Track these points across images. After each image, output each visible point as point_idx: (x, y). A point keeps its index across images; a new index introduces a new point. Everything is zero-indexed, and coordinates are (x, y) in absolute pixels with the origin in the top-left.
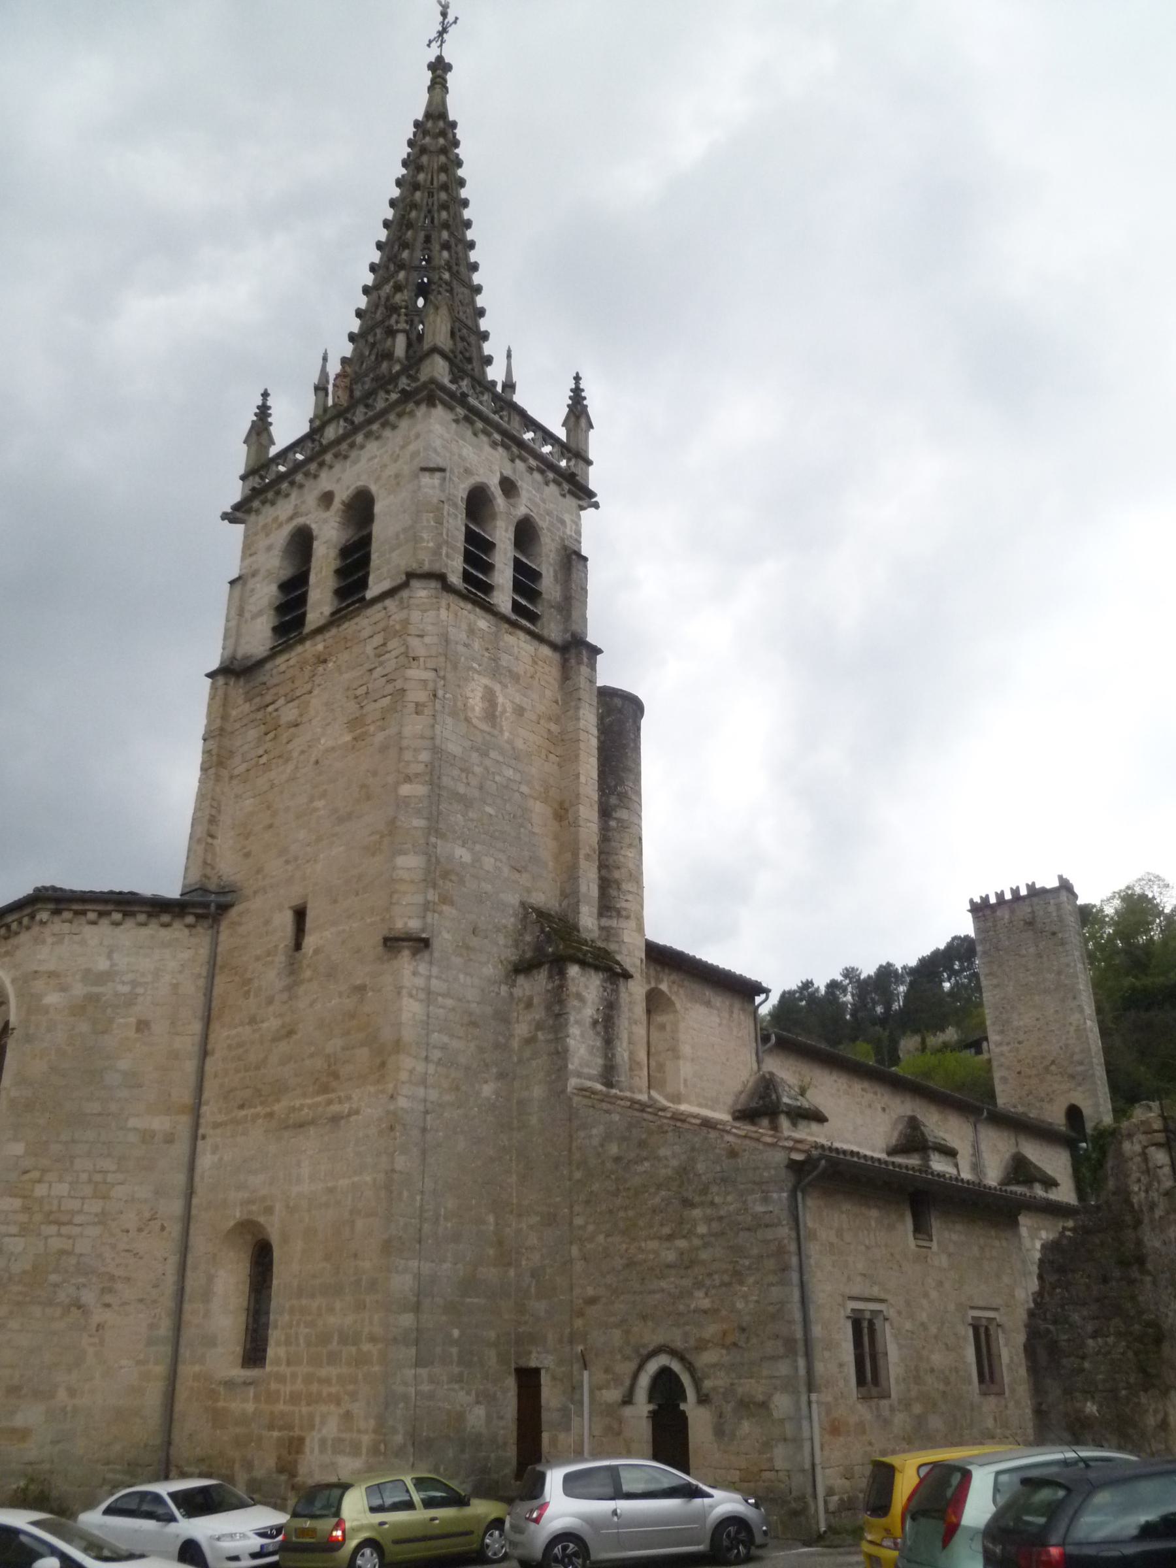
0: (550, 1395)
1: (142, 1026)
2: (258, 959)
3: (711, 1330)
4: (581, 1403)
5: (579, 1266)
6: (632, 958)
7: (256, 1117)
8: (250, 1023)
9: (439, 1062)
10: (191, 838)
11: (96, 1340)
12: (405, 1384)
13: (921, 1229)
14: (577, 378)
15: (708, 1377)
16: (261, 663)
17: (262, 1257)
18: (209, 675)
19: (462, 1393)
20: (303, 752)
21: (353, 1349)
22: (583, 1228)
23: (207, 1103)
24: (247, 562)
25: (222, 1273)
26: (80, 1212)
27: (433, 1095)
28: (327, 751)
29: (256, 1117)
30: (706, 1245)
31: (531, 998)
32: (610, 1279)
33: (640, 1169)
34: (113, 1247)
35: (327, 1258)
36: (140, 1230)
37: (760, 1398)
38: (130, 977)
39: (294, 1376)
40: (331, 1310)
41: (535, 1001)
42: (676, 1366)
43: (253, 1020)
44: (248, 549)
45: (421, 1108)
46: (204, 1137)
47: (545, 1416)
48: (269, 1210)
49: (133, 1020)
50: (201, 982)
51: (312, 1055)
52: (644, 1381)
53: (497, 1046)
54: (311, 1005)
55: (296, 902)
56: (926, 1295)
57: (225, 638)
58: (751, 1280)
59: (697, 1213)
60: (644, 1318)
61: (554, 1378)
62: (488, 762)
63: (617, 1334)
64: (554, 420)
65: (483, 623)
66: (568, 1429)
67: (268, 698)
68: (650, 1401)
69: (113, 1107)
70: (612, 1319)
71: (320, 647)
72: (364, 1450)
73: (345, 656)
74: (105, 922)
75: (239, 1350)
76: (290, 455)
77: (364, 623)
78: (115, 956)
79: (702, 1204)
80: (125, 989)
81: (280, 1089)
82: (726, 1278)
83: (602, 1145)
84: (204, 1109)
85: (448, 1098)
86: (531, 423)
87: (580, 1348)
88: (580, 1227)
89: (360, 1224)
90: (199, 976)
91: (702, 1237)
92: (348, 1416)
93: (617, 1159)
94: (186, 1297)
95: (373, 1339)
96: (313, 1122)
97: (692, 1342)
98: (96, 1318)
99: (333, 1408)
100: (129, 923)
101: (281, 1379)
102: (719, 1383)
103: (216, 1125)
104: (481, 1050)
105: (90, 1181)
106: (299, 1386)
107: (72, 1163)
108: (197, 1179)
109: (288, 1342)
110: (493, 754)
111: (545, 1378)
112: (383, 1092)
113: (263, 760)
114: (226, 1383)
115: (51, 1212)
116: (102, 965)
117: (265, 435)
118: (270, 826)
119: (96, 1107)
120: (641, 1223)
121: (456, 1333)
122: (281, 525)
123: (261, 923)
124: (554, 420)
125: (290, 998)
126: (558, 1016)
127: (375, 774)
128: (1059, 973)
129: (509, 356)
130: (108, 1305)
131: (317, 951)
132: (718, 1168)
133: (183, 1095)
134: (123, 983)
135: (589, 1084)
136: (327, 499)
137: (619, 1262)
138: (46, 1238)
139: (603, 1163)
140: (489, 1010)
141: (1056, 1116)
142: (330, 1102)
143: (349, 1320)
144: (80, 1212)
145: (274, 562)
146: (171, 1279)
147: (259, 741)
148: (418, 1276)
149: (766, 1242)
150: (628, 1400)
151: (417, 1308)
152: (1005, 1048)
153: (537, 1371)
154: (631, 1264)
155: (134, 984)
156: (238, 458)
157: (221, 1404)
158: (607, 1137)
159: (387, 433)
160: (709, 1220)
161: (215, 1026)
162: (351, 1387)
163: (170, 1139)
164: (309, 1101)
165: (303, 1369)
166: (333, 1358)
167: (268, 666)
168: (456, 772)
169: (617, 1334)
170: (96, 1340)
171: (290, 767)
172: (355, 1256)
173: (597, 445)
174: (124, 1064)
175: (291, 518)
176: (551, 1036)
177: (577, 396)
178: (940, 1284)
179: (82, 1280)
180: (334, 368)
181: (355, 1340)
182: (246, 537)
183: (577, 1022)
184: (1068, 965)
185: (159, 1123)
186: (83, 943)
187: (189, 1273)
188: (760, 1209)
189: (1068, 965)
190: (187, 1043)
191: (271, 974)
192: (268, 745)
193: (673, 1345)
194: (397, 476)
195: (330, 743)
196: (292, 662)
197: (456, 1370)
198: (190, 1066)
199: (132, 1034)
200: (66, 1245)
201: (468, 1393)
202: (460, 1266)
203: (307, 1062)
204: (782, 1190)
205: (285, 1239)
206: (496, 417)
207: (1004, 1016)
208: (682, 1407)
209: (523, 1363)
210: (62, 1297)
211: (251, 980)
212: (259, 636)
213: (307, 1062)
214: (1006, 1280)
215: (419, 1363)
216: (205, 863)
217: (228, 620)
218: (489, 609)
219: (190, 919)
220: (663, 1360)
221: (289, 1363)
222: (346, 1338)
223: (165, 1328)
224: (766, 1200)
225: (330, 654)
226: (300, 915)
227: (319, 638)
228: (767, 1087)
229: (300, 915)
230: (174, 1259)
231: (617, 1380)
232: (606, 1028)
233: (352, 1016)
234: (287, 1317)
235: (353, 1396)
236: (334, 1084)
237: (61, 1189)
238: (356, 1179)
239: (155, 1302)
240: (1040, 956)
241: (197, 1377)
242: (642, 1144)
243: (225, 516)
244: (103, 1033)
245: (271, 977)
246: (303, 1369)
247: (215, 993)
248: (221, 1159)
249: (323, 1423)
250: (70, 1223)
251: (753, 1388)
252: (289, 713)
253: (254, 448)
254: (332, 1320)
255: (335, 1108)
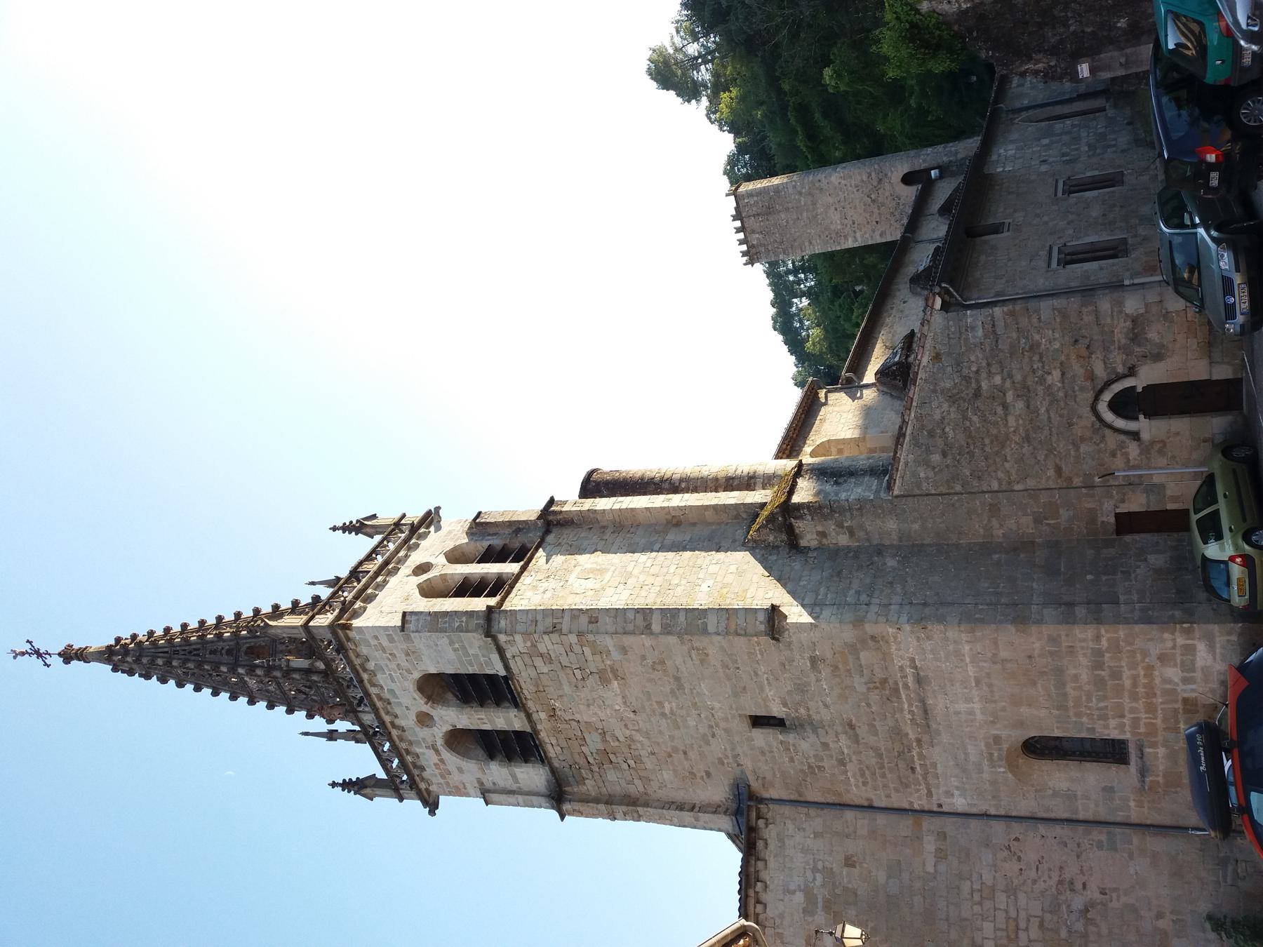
0: (1136, 503)
1: (849, 862)
2: (792, 760)
3: (1077, 368)
4: (1141, 476)
5: (1031, 483)
6: (789, 464)
7: (922, 757)
8: (845, 765)
9: (870, 596)
10: (695, 827)
11: (1114, 895)
12: (1132, 611)
13: (997, 229)
14: (334, 529)
15: (1114, 369)
16: (553, 771)
17: (1039, 748)
18: (562, 818)
19: (1138, 571)
20: (626, 726)
21: (1107, 655)
22: (1000, 481)
23: (911, 803)
24: (471, 791)
25: (1051, 784)
26: (1006, 911)
27: (896, 599)
28: (625, 703)
29: (922, 757)
30: (1010, 376)
31: (819, 533)
32: (1041, 457)
33: (951, 434)
34: (1034, 882)
35: (1034, 683)
36: (1019, 859)
37: (1129, 323)
38: (809, 874)
39: (1132, 710)
40: (1076, 677)
41: (820, 529)
42: (1107, 396)
43: (842, 762)
44: (459, 791)
45: (907, 607)
46: (940, 806)
47: (1154, 508)
48: (997, 739)
49: (845, 870)
50: (813, 812)
51: (869, 705)
52: (1120, 423)
53: (856, 557)
54: (826, 706)
55: (746, 724)
56: (1046, 223)
57: (533, 806)
58: (1037, 337)
59: (984, 385)
60: (1070, 425)
61: (1123, 501)
62: (635, 572)
63: (1084, 448)
64: (364, 544)
65: (526, 579)
66: (1163, 486)
67: (582, 761)
68: (1137, 419)
69: (918, 885)
70: (1073, 453)
71: (543, 715)
72: (1190, 642)
73: (551, 691)
74: (763, 897)
75: (1114, 767)
76: (385, 756)
77: (525, 682)
78: (792, 887)
79: (978, 381)
80: (819, 877)
81: (897, 733)
82: (1036, 358)
83: (934, 468)
84: (916, 807)
85: (899, 589)
86: (369, 558)
87: (1097, 479)
88: (1000, 484)
89: (1004, 654)
90: (807, 815)
91: (1004, 380)
92: (1163, 658)
93: (944, 454)
94: (1074, 817)
95: (1098, 638)
96: (923, 701)
97: (1088, 384)
98: (1097, 896)
99: (1157, 673)
100: (764, 875)
101: (1135, 722)
102: (1119, 360)
103: (930, 794)
104: (860, 568)
105: (980, 904)
106: (1140, 705)
107: (966, 919)
108: (974, 810)
109: (1104, 717)
110: (630, 569)
111: (1123, 509)
112: (895, 638)
113: (631, 762)
114: (1143, 776)
115: (1008, 936)
116: (799, 898)
117: (367, 782)
118: (685, 753)
119: (918, 900)
120: (995, 431)
121: (1089, 577)
122: (442, 761)
123: (763, 757)
124: (364, 544)
125: (823, 727)
126: (832, 510)
127: (643, 658)
128: (800, 193)
129: (313, 583)
130: (1084, 885)
131: (785, 705)
132: (949, 369)
133: (905, 826)
134: (814, 879)
135: (884, 484)
136: (424, 719)
137: (1026, 449)
138: (1030, 941)
139: (947, 466)
140: (828, 564)
141: (909, 193)
142: (906, 686)
143: (1083, 660)
144: (1006, 911)
145: (470, 769)
146: (1059, 830)
147: (616, 767)
148: (1045, 605)
149: (1006, 326)
150: (1135, 435)
151: (1070, 605)
152: (858, 234)
153: (1117, 516)
154: (1027, 439)
155: (815, 870)
156: (385, 804)
157: (1160, 779)
158: (927, 464)
159: (371, 665)
160: (990, 375)
161: (847, 799)
162: (1139, 657)
163: (942, 836)
164: (906, 706)
165: (1127, 703)
166: (1116, 674)
167: (556, 764)
168: (643, 593)
169: (1084, 448)
170: (1114, 895)
171: (638, 737)
172: (1030, 657)
173: (387, 516)
174: (881, 877)
175: (437, 751)
176: (848, 514)
177: (348, 528)
178: (1037, 216)
179: (1064, 908)
180: (319, 724)
181: (1099, 653)
182: (450, 794)
183: (836, 495)
184: (795, 187)
185: (930, 844)
186: (781, 916)
187: (1052, 815)
188: (980, 333)
189: (795, 187)
190: (862, 822)
191: (804, 746)
192: (620, 760)
193: (1091, 400)
194: (407, 654)
195: (619, 700)
196: (554, 742)
197: (1119, 576)
198: (881, 820)
199: (856, 871)
200: (1035, 923)
201: (1139, 567)
202: (1035, 576)
203: (874, 709)
204: (965, 315)
205: (1021, 724)
206: (364, 581)
207: (833, 235)
208: (1139, 390)
209: (1112, 528)
210: (1079, 926)
211: (810, 767)
212: (532, 775)
213: (874, 709)
214: (1033, 177)
215: (1116, 602)
216: (715, 812)
217: (518, 805)
218: (518, 577)
219: (761, 823)
220: (1103, 407)
221: (1123, 716)
222: (1098, 665)
223: (1099, 835)
224: (973, 328)
225: (548, 705)
226: (758, 721)
227: (535, 716)
228: (887, 375)
229: (758, 721)
230: (1042, 829)
231: (1121, 446)
232: (841, 476)
233: (836, 668)
234: (1084, 719)
235: (1145, 654)
236: (891, 681)
237: (988, 927)
238: (968, 660)
239: (1079, 845)
240: (787, 209)
241: (1140, 804)
242: (931, 434)
243: (432, 813)
244: (856, 894)
245: (806, 745)
246: (1127, 703)
247: (822, 800)
248: (957, 788)
249: (1169, 681)
250: (1016, 920)
251: (1120, 330)
252: (594, 742)
253: (378, 791)
254: (1085, 676)
255: (910, 680)
